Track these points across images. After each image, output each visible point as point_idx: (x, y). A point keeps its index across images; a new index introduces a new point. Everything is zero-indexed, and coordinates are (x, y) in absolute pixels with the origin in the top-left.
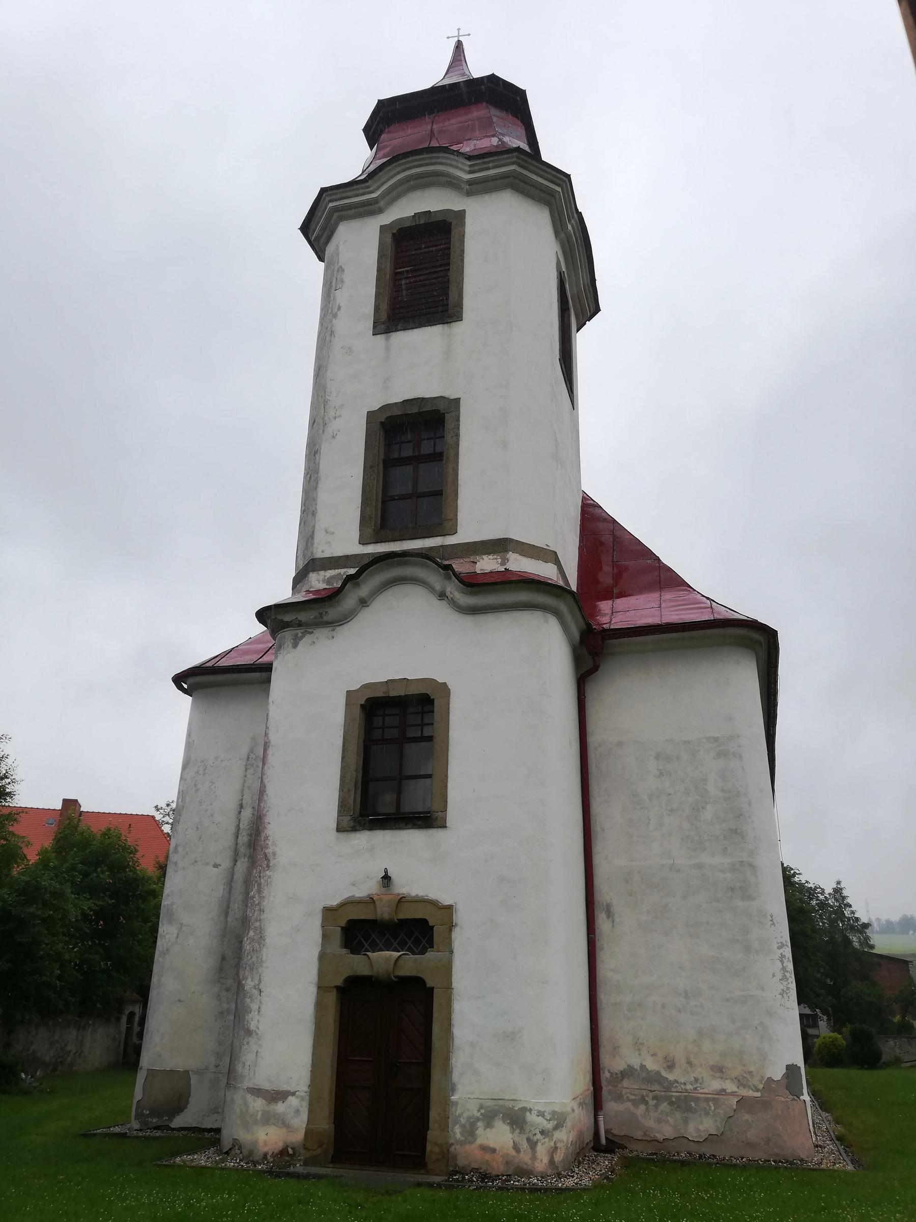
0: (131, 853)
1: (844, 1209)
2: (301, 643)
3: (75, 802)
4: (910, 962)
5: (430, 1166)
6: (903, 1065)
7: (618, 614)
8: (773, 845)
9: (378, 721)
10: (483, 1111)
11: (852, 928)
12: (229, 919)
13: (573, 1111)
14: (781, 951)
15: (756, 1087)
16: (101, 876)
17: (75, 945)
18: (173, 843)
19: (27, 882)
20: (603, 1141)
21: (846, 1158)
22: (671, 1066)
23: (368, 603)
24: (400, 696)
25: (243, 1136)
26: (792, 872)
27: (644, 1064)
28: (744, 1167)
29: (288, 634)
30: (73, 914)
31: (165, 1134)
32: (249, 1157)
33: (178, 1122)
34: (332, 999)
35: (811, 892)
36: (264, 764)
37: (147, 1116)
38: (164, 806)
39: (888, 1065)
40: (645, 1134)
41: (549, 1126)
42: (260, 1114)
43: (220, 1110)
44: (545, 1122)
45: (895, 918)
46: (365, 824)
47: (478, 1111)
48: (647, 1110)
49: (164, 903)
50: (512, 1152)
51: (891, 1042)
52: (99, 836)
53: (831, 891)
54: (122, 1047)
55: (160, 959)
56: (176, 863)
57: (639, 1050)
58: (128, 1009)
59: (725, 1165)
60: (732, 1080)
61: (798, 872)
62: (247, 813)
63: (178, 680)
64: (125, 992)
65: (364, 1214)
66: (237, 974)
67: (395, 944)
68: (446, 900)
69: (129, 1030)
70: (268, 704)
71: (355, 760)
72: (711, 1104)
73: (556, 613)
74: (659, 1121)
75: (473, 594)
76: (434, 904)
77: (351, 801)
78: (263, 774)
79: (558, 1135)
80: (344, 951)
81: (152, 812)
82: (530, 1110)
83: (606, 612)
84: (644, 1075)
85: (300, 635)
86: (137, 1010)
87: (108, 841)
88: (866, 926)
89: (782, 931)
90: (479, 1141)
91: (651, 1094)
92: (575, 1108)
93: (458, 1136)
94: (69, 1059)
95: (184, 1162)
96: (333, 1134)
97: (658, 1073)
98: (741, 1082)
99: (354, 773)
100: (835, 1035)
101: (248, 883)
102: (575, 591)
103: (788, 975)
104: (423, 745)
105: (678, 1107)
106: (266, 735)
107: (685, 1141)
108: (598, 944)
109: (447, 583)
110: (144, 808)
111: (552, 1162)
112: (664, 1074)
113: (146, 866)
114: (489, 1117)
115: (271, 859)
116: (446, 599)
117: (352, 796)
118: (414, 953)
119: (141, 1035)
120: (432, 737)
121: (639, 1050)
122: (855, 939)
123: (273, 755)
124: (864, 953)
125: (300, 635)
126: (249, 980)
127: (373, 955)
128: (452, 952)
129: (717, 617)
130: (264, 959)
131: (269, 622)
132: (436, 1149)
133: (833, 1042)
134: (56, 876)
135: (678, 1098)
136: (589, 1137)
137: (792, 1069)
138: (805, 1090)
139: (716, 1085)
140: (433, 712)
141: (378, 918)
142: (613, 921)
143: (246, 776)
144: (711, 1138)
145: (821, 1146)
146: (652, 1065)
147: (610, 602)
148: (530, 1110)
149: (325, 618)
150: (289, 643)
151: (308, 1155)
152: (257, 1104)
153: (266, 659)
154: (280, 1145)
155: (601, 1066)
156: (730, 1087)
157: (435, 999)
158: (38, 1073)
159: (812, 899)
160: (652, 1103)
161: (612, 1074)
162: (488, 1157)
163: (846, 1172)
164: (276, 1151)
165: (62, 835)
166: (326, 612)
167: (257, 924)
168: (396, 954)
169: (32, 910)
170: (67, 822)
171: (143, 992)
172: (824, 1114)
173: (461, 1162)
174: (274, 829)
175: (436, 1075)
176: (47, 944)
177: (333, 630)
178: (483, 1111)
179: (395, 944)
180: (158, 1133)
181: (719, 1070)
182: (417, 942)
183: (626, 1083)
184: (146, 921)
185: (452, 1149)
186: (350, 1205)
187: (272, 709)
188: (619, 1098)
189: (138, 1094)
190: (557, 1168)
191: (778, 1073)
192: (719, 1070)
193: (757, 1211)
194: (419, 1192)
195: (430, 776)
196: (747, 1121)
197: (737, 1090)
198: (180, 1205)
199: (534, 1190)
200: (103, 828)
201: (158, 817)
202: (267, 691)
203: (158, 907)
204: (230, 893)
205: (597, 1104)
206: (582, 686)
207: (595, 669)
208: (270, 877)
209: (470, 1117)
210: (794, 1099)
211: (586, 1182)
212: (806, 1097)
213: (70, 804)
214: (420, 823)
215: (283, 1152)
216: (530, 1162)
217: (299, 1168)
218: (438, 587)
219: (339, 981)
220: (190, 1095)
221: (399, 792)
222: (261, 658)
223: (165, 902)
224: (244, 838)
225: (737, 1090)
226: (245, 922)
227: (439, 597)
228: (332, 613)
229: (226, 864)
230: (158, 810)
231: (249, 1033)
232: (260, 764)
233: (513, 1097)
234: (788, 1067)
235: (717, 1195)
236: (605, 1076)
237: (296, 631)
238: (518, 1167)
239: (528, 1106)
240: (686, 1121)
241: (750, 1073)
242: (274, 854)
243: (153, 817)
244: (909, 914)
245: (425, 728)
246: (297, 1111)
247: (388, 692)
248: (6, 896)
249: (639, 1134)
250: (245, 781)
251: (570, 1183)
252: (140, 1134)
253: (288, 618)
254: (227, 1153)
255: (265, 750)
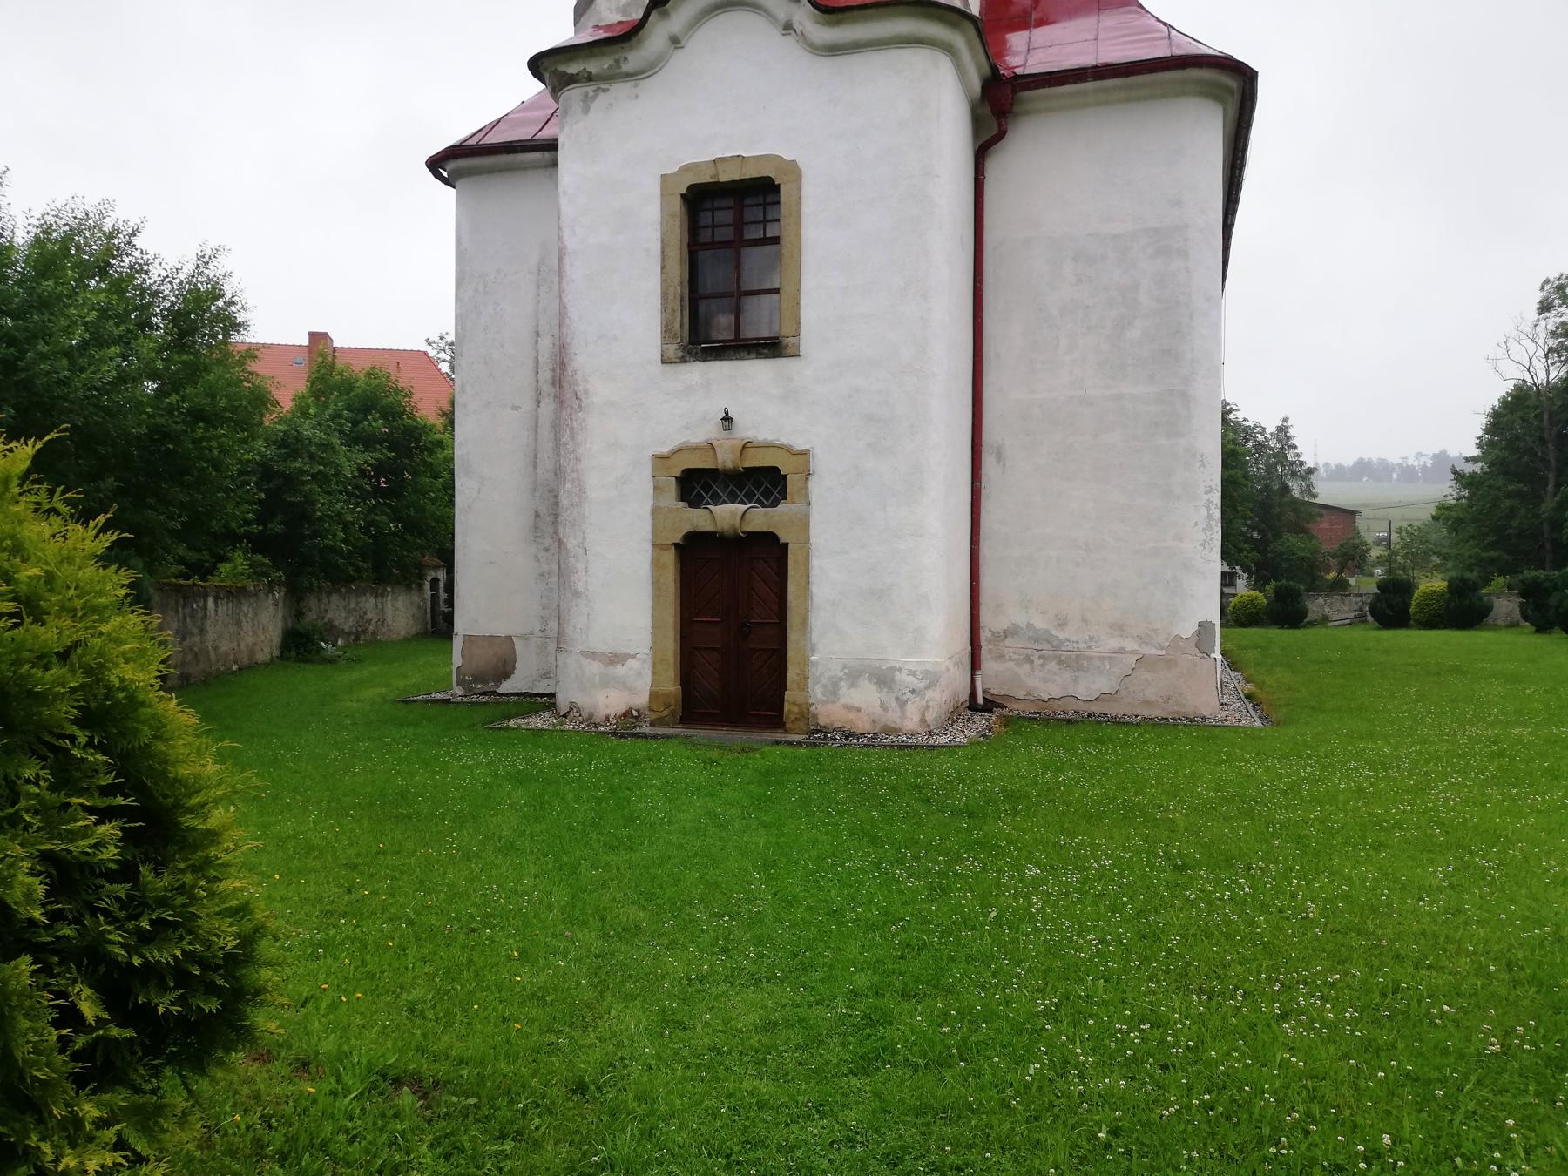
0: (405, 396)
1: (1247, 762)
2: (595, 106)
3: (325, 335)
4: (1357, 512)
5: (788, 726)
6: (1330, 624)
7: (1037, 51)
8: (1216, 370)
9: (705, 218)
10: (846, 671)
11: (1294, 474)
12: (538, 470)
13: (948, 670)
14: (1209, 495)
15: (1160, 645)
16: (374, 424)
17: (357, 505)
18: (457, 383)
19: (285, 432)
20: (980, 701)
21: (1253, 715)
22: (1062, 625)
23: (682, 44)
24: (733, 181)
25: (581, 700)
26: (1228, 408)
27: (1032, 622)
28: (1138, 725)
29: (574, 93)
30: (348, 471)
31: (493, 699)
32: (589, 719)
33: (506, 687)
34: (670, 557)
35: (1248, 432)
36: (561, 276)
37: (471, 682)
38: (437, 340)
39: (1312, 624)
40: (1028, 694)
41: (922, 685)
42: (597, 677)
43: (551, 675)
44: (916, 681)
45: (1348, 461)
46: (696, 353)
47: (842, 671)
48: (1032, 669)
49: (457, 453)
50: (879, 711)
51: (1321, 600)
52: (362, 376)
53: (1274, 430)
54: (429, 615)
55: (462, 517)
56: (465, 406)
57: (1027, 607)
58: (431, 575)
59: (1117, 723)
60: (1133, 637)
61: (1235, 407)
62: (546, 343)
63: (435, 164)
64: (424, 556)
65: (720, 770)
66: (556, 532)
67: (741, 496)
68: (800, 445)
69: (435, 597)
70: (556, 196)
71: (678, 270)
72: (1107, 663)
73: (949, 49)
74: (1045, 680)
75: (830, 24)
76: (786, 449)
77: (677, 325)
78: (561, 291)
79: (929, 694)
80: (681, 504)
81: (424, 347)
82: (900, 670)
83: (1019, 49)
84: (1031, 633)
85: (591, 94)
86: (441, 575)
87: (374, 383)
88: (1311, 471)
89: (1213, 474)
90: (843, 701)
91: (1037, 654)
92: (951, 666)
93: (819, 695)
94: (371, 628)
95: (519, 725)
96: (680, 695)
97: (1047, 631)
98: (1142, 639)
99: (679, 289)
100: (1256, 593)
101: (557, 427)
102: (977, 15)
103: (1213, 523)
104: (767, 249)
105: (1068, 666)
106: (560, 238)
107: (1074, 700)
108: (984, 492)
109: (794, 7)
110: (411, 341)
111: (923, 721)
112: (1054, 632)
113: (427, 412)
114: (853, 677)
115: (583, 397)
116: (792, 32)
117: (679, 319)
118: (764, 506)
119: (450, 602)
120: (778, 237)
121: (1027, 607)
122: (1295, 488)
123: (571, 265)
124: (1304, 503)
125: (591, 94)
126: (572, 537)
127: (717, 509)
128: (809, 504)
129: (1177, 52)
130: (587, 514)
131: (547, 75)
132: (796, 709)
133: (1251, 602)
134: (319, 424)
135: (1069, 657)
136: (964, 695)
137: (1204, 627)
138: (1217, 648)
139: (1113, 643)
140: (778, 203)
141: (720, 467)
142: (1004, 465)
143: (539, 295)
144: (1103, 697)
145: (1226, 704)
146: (1039, 623)
147: (1025, 34)
148: (900, 670)
149: (625, 68)
150: (577, 107)
151: (654, 716)
152: (594, 668)
153: (547, 133)
154: (623, 708)
155: (981, 625)
156: (1130, 645)
157: (790, 555)
158: (339, 643)
159: (1247, 440)
160: (1038, 662)
161: (993, 633)
162: (852, 715)
163: (1252, 728)
164: (619, 714)
165: (317, 375)
166: (625, 59)
167: (574, 475)
168: (743, 507)
169: (298, 464)
170: (320, 359)
171: (447, 558)
172: (1233, 674)
173: (823, 721)
174: (583, 360)
175: (793, 636)
176: (323, 504)
177: (636, 86)
178: (846, 671)
179: (741, 496)
180: (486, 699)
181: (1119, 628)
182: (767, 494)
183: (1008, 642)
184: (436, 477)
185: (813, 709)
186: (705, 763)
187: (564, 202)
188: (1000, 657)
189: (457, 660)
190: (928, 726)
191: (1188, 629)
192: (1119, 628)
193: (1150, 764)
194: (778, 750)
195: (777, 291)
196: (1146, 680)
197: (1137, 648)
198: (521, 764)
199: (903, 747)
200: (367, 367)
201: (432, 353)
202: (554, 179)
203: (450, 460)
204: (536, 440)
205: (975, 664)
206: (981, 160)
207: (1001, 136)
208: (584, 420)
209: (832, 677)
210: (1203, 657)
211: (960, 739)
212: (1218, 656)
213: (318, 338)
214: (766, 351)
215: (627, 714)
216: (898, 721)
217: (645, 729)
218: (782, 17)
219: (678, 538)
220: (515, 661)
221: (738, 312)
222: (540, 130)
223: (459, 453)
224: (545, 375)
225: (1137, 648)
226: (559, 472)
227: (784, 30)
228: (634, 58)
229: (527, 405)
230: (430, 344)
231: (577, 594)
232: (556, 279)
233: (880, 657)
234: (1201, 624)
235: (1107, 750)
236: (984, 635)
237: (585, 89)
238: (886, 725)
239: (898, 665)
240: (1076, 680)
241: (1155, 630)
242: (586, 392)
243: (425, 353)
244: (1366, 458)
245: (769, 226)
246: (639, 674)
247: (717, 175)
248: (264, 450)
249: (1021, 694)
250: (538, 302)
251: (942, 740)
252: (466, 700)
253: (573, 68)
254: (565, 716)
255: (561, 260)
